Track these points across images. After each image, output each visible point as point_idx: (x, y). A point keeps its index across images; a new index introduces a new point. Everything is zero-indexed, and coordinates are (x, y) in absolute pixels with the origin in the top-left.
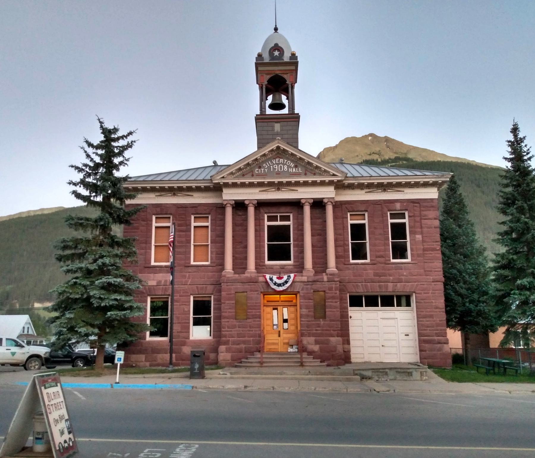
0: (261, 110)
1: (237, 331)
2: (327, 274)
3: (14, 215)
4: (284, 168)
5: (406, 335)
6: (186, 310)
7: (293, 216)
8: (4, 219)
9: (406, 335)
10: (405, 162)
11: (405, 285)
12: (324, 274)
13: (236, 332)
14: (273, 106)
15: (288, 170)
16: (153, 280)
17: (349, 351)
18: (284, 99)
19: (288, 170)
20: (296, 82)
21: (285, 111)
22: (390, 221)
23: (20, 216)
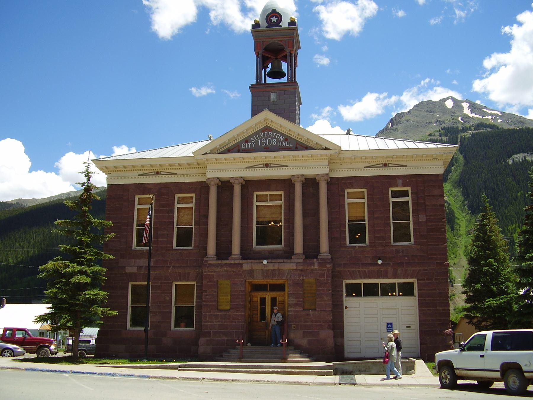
0: (257, 79)
1: (219, 322)
2: (318, 260)
3: (56, 196)
4: (272, 141)
5: (407, 327)
6: (168, 298)
7: (392, 187)
8: (45, 201)
9: (407, 327)
10: (489, 129)
11: (152, 312)
12: (315, 260)
13: (218, 323)
14: (272, 75)
15: (277, 143)
16: (134, 266)
17: (342, 346)
18: (284, 66)
19: (277, 143)
20: (299, 48)
21: (284, 80)
22: (392, 200)
23: (59, 198)
